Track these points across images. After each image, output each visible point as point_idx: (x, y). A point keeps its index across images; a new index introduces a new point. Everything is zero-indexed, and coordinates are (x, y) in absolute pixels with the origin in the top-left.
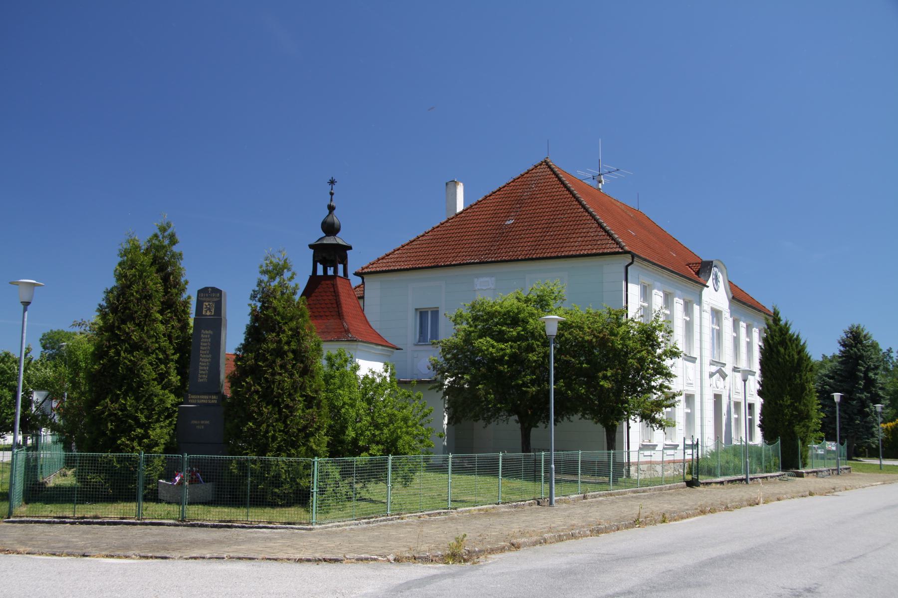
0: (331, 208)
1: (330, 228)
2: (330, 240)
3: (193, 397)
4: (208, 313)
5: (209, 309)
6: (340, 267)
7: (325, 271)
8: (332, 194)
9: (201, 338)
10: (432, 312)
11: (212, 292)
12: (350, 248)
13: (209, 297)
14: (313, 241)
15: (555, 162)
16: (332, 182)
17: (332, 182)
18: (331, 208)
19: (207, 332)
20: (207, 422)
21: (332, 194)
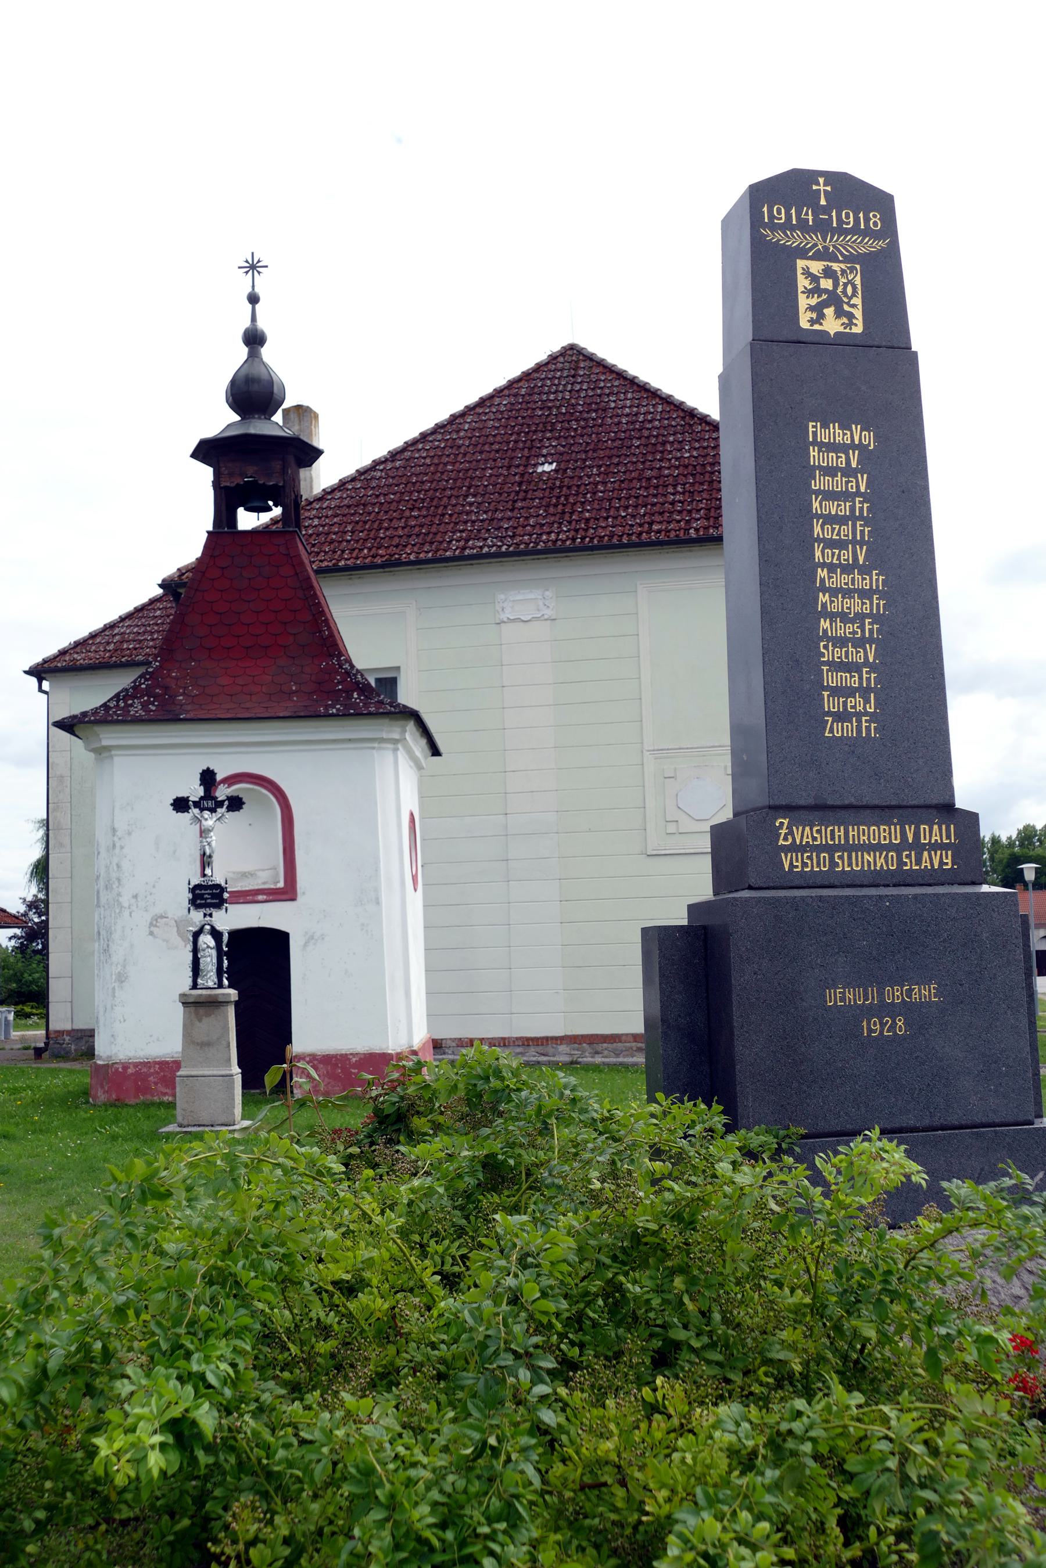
0: (254, 339)
3: (804, 835)
5: (834, 300)
9: (809, 471)
13: (823, 227)
16: (253, 267)
18: (254, 339)
19: (836, 434)
20: (925, 993)
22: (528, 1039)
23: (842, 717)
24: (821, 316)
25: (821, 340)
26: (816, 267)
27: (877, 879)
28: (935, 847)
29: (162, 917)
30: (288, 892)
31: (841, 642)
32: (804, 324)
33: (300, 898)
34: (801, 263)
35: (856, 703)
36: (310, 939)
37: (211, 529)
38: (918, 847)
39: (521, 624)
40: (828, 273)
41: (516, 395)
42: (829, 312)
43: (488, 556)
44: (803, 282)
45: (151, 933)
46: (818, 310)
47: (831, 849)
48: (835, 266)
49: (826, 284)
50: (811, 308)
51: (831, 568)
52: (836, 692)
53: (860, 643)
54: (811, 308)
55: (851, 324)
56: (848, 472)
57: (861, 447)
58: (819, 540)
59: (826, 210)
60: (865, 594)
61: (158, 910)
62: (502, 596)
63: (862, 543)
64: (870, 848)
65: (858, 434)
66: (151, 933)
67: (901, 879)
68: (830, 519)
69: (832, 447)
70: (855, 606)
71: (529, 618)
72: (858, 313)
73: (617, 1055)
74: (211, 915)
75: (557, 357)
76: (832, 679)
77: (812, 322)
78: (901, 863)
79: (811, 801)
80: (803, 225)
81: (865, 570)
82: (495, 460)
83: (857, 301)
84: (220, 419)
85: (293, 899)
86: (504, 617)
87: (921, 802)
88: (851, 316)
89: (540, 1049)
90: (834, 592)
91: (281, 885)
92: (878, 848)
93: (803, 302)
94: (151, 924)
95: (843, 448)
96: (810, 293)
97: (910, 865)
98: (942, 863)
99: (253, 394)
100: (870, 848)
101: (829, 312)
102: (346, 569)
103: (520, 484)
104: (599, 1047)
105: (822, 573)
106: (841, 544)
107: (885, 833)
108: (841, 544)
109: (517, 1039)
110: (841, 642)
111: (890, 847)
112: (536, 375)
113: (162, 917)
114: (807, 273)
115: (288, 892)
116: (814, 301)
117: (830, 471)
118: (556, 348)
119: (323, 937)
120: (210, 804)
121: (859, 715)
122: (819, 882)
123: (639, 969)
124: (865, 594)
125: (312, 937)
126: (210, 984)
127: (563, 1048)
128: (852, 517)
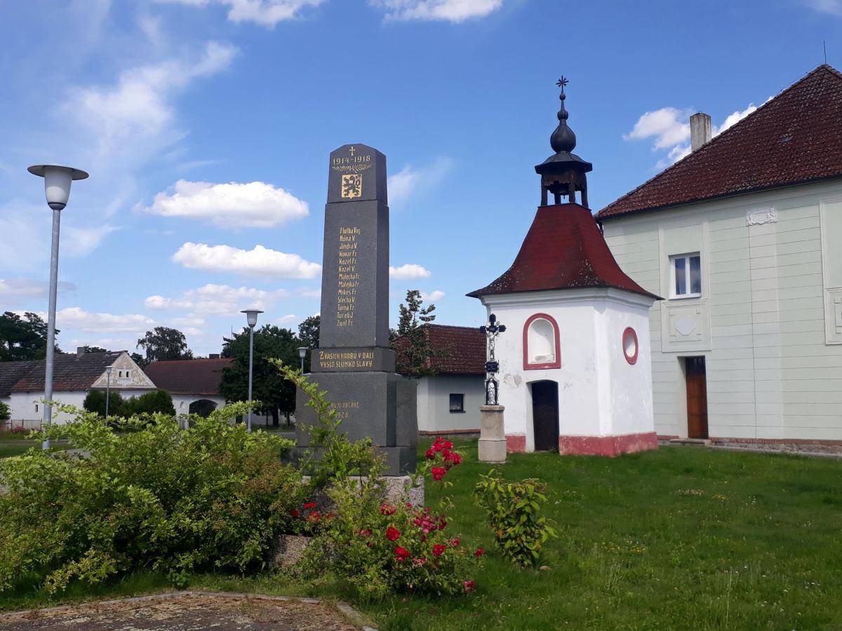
0: (563, 116)
1: (563, 142)
2: (564, 157)
3: (328, 356)
4: (351, 195)
5: (353, 187)
6: (578, 194)
7: (558, 200)
8: (562, 98)
9: (339, 243)
10: (691, 259)
11: (356, 154)
12: (588, 167)
13: (351, 163)
14: (541, 161)
15: (670, 254)
16: (562, 82)
17: (562, 82)
18: (563, 116)
19: (350, 231)
20: (355, 405)
21: (562, 98)
22: (765, 440)
23: (342, 320)
24: (348, 193)
25: (348, 201)
26: (348, 177)
27: (348, 370)
28: (366, 360)
29: (509, 375)
30: (557, 365)
31: (344, 297)
32: (343, 196)
33: (562, 367)
34: (344, 176)
35: (347, 316)
36: (567, 385)
37: (540, 205)
38: (361, 360)
39: (758, 226)
40: (352, 178)
41: (785, 99)
42: (351, 191)
43: (740, 192)
44: (344, 182)
45: (505, 382)
46: (348, 191)
47: (335, 361)
48: (354, 176)
49: (351, 182)
50: (345, 191)
51: (343, 273)
52: (341, 312)
53: (350, 297)
54: (345, 191)
55: (357, 194)
56: (351, 243)
57: (356, 234)
58: (340, 265)
59: (353, 157)
60: (353, 281)
61: (507, 373)
62: (750, 212)
63: (354, 265)
64: (347, 360)
65: (355, 230)
66: (505, 382)
67: (356, 370)
68: (344, 258)
69: (347, 235)
70: (350, 285)
71: (763, 222)
72: (360, 190)
73: (811, 450)
74: (493, 375)
75: (813, 74)
76: (340, 309)
77: (345, 195)
78: (356, 364)
79: (331, 346)
80: (346, 164)
81: (354, 274)
82: (762, 138)
83: (360, 186)
84: (546, 153)
85: (559, 368)
86: (750, 222)
87: (364, 345)
88: (358, 191)
89: (771, 446)
90: (343, 281)
91: (555, 361)
92: (350, 360)
93: (343, 188)
94: (505, 378)
95: (350, 235)
96: (345, 186)
97: (359, 365)
98: (369, 365)
99: (563, 142)
100: (347, 360)
101: (351, 191)
102: (673, 204)
103: (771, 149)
104: (801, 446)
105: (341, 275)
106: (347, 266)
107: (351, 356)
108: (347, 266)
109: (759, 439)
110: (344, 297)
111: (353, 359)
112: (799, 86)
113: (509, 375)
114: (345, 179)
115: (557, 365)
116: (346, 188)
117: (346, 243)
118: (812, 69)
119: (571, 384)
120: (493, 329)
121: (348, 319)
122: (331, 370)
123: (708, 401)
124: (353, 281)
125: (567, 384)
126: (492, 403)
127: (783, 446)
128: (351, 257)
